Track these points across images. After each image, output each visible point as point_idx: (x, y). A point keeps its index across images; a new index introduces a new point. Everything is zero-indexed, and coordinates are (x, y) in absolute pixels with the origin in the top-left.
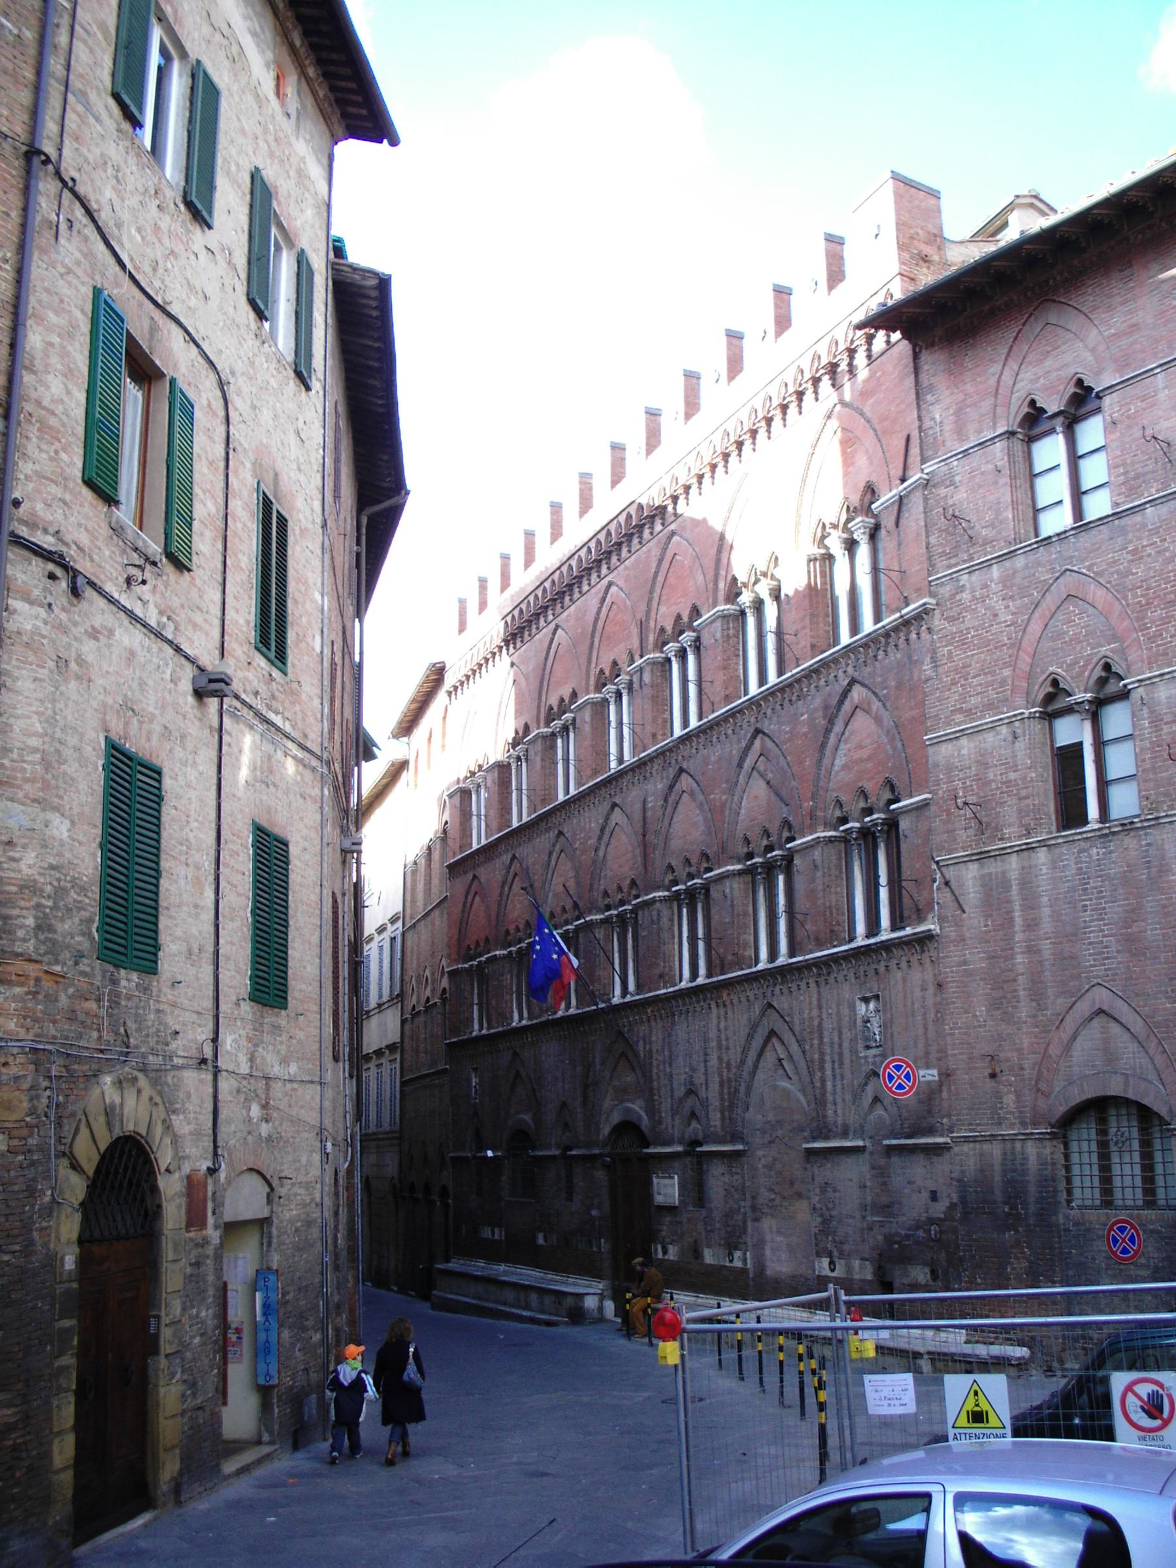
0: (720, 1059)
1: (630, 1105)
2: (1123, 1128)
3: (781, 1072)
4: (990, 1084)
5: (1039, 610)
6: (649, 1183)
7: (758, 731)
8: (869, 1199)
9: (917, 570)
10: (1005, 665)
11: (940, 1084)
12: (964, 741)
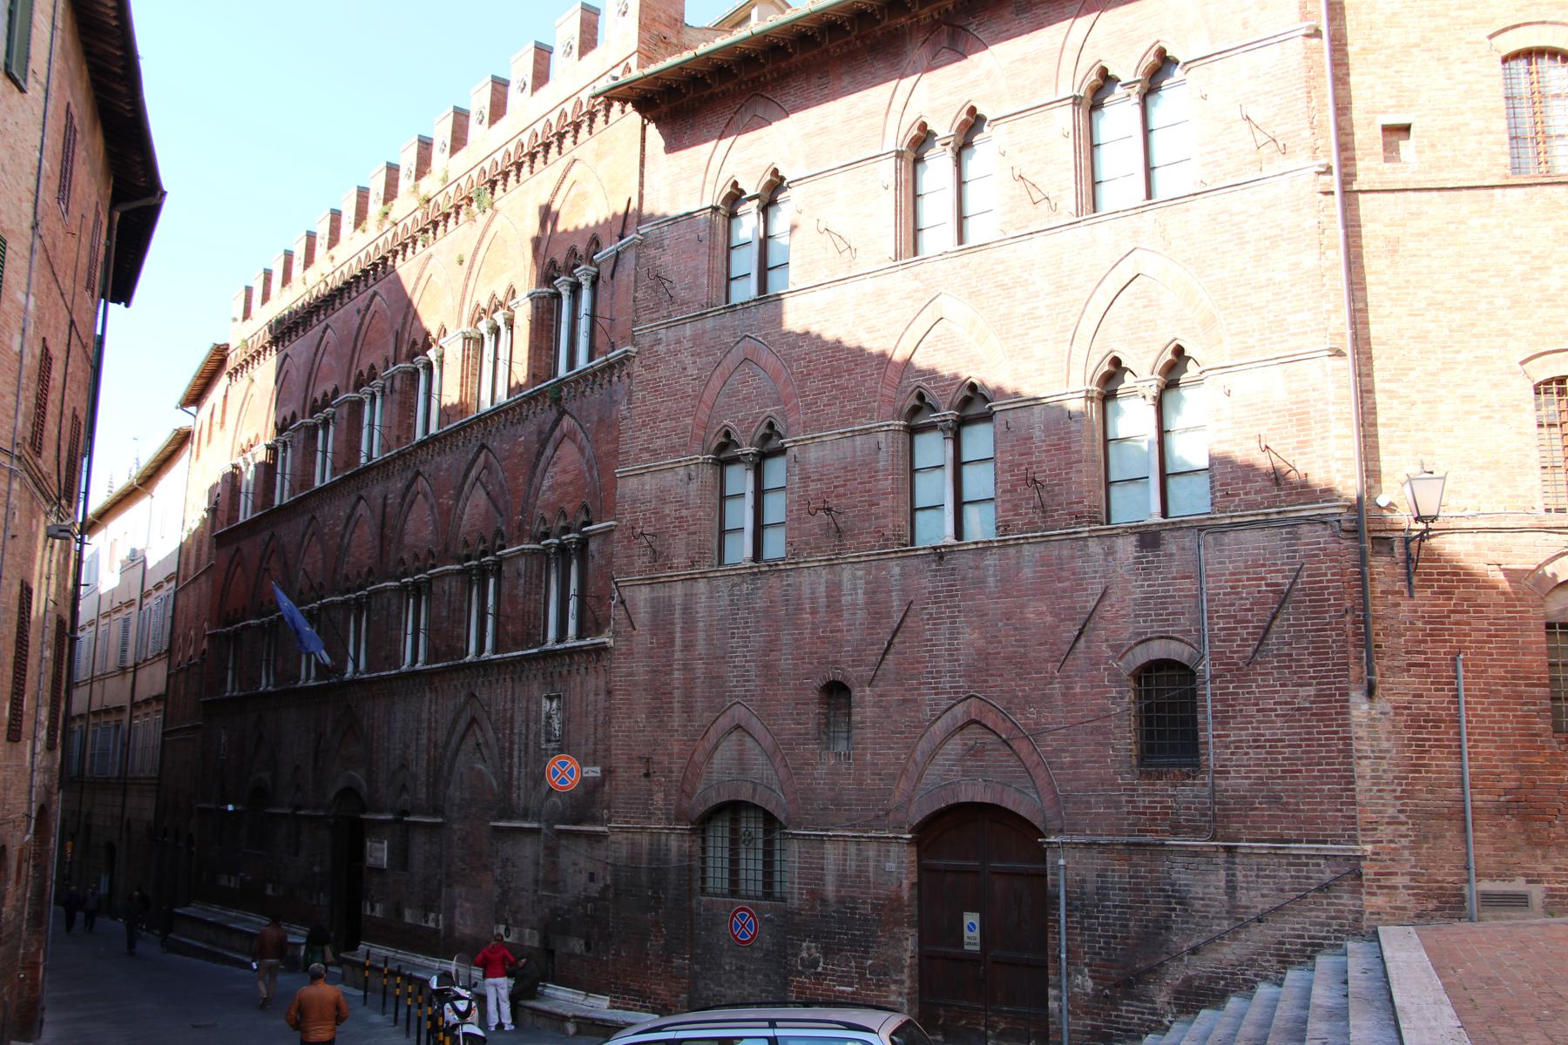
0: (429, 739)
1: (352, 773)
2: (752, 827)
3: (478, 755)
4: (644, 782)
5: (720, 368)
6: (363, 846)
7: (483, 446)
8: (541, 875)
9: (623, 319)
10: (689, 414)
11: (603, 778)
12: (647, 477)
